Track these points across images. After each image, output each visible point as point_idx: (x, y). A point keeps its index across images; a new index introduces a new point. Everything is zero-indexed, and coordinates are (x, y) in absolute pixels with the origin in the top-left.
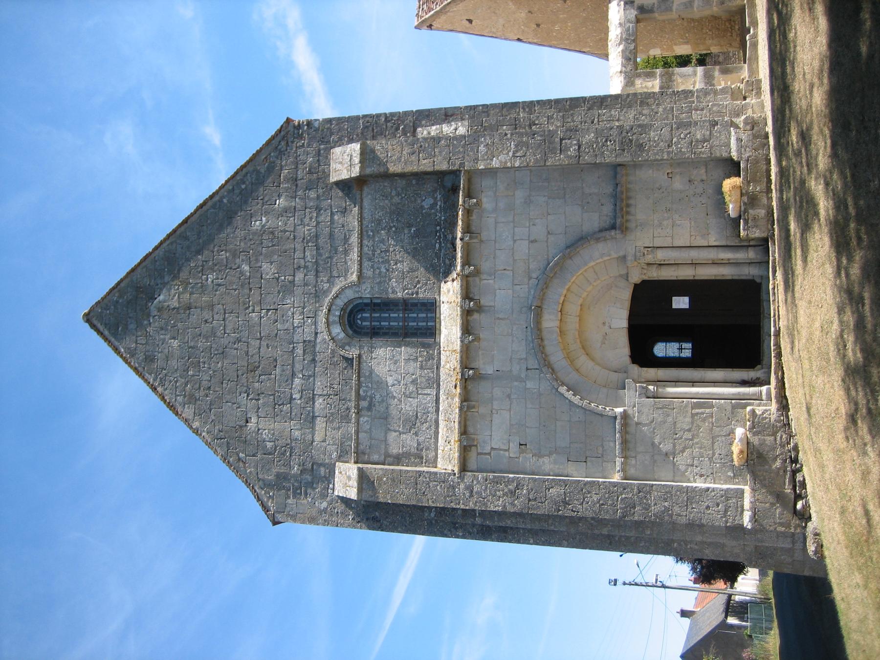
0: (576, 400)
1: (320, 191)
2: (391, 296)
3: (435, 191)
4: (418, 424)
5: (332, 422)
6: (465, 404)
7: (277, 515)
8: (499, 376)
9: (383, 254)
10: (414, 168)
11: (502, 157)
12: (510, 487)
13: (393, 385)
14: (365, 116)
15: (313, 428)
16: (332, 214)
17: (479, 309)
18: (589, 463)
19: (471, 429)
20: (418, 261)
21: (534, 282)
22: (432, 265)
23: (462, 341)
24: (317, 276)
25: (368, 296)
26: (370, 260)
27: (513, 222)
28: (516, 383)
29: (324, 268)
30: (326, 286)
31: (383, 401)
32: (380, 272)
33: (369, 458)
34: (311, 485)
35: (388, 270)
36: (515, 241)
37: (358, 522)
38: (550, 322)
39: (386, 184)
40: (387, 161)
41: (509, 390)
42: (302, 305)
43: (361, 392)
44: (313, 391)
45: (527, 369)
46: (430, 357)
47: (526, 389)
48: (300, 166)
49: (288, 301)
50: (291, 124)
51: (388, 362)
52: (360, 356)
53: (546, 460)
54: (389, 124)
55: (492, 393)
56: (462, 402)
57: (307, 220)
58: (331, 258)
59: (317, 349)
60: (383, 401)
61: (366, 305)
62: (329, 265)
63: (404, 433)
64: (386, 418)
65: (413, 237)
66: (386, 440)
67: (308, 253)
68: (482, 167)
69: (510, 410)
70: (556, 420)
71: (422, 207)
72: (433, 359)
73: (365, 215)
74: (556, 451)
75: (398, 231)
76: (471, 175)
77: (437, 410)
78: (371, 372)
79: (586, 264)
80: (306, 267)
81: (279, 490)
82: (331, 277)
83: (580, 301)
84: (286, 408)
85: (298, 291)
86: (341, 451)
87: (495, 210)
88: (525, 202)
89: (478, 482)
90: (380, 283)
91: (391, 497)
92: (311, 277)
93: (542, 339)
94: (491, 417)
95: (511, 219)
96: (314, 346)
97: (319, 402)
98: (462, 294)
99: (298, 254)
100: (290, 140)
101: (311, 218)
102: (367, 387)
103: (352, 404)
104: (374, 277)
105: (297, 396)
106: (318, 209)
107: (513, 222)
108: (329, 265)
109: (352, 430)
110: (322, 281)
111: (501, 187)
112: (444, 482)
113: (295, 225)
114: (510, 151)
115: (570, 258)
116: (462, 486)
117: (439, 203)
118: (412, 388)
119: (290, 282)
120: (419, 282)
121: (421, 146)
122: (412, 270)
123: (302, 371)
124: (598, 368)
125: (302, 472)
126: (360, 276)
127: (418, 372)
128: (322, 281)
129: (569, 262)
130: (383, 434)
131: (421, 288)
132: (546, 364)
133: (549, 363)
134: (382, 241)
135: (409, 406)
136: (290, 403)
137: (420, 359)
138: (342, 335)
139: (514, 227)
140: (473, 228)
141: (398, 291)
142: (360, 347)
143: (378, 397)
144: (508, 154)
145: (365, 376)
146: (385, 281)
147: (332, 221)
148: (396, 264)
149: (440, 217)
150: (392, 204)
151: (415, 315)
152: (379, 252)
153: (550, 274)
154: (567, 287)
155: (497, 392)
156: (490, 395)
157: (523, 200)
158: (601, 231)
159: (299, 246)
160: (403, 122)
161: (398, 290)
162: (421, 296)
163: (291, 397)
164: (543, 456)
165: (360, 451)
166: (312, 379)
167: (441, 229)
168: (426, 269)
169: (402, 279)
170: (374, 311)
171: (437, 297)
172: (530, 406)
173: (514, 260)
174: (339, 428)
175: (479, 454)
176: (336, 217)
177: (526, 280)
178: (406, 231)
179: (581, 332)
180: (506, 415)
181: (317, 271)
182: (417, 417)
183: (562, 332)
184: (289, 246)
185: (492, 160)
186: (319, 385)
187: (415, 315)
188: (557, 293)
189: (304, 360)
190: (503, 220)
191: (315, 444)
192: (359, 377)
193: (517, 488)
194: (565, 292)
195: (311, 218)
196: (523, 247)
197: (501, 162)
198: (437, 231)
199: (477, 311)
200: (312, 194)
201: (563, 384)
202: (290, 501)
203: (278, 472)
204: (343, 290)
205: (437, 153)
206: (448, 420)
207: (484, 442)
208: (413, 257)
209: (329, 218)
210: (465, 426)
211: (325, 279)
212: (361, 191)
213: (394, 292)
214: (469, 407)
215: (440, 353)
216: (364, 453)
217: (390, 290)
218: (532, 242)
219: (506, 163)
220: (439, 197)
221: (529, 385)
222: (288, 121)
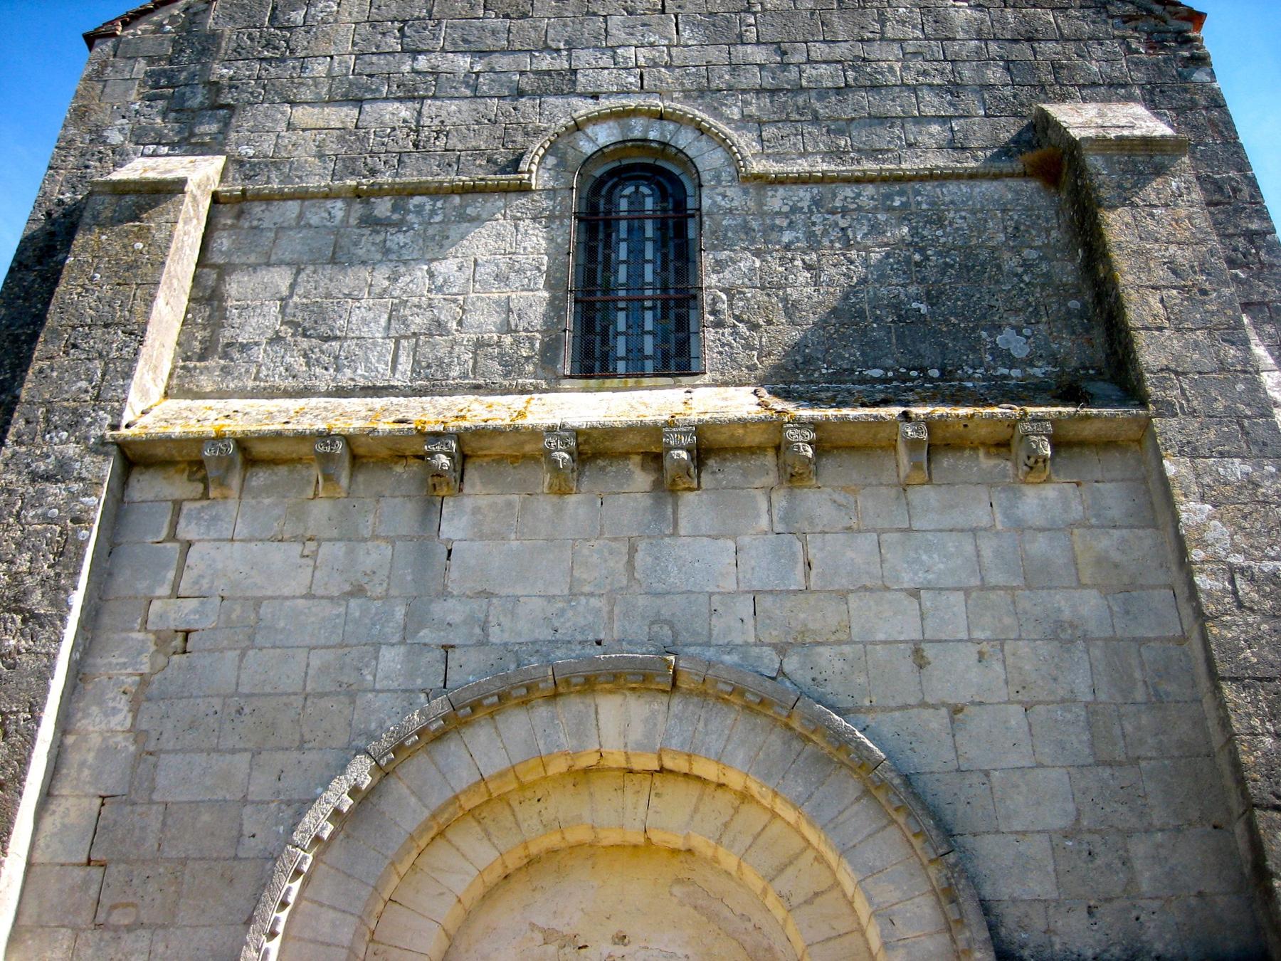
0: (318, 822)
1: (1008, 92)
2: (707, 259)
3: (1053, 359)
4: (305, 343)
5: (341, 139)
6: (340, 447)
7: (110, 42)
8: (429, 555)
9: (835, 234)
10: (1127, 273)
11: (1218, 531)
12: (37, 595)
13: (431, 275)
14: (1253, 183)
15: (331, 102)
16: (943, 120)
17: (668, 487)
18: (79, 874)
19: (260, 477)
20: (822, 324)
21: (769, 661)
22: (808, 360)
23: (551, 430)
24: (759, 91)
25: (706, 203)
26: (817, 203)
27: (984, 587)
28: (400, 612)
29: (783, 106)
30: (735, 113)
31: (387, 252)
32: (781, 229)
33: (225, 227)
34: (177, 109)
35: (787, 247)
36: (915, 593)
37: (49, 214)
38: (620, 724)
39: (1054, 234)
40: (1134, 205)
41: (379, 590)
42: (677, 62)
43: (417, 200)
44: (434, 97)
45: (446, 648)
46: (510, 366)
47: (377, 646)
48: (1071, 46)
49: (686, 34)
50: (1187, 25)
51: (508, 263)
52: (524, 189)
53: (122, 720)
54: (1241, 243)
55: (375, 537)
56: (348, 439)
57: (917, 64)
58: (816, 120)
59: (551, 100)
60: (387, 252)
61: (680, 205)
62: (795, 116)
63: (283, 309)
64: (333, 261)
65: (896, 306)
66: (268, 265)
67: (823, 69)
68: (1170, 468)
69: (309, 596)
70: (257, 753)
71: (998, 328)
72: (506, 375)
73: (952, 187)
74: (146, 752)
75: (912, 270)
76: (1143, 445)
77: (341, 392)
78: (477, 220)
79: (844, 852)
80: (784, 66)
81: (174, 42)
82: (761, 123)
83: (700, 842)
84: (393, 43)
85: (716, 54)
86: (253, 166)
87: (1020, 527)
88: (1060, 625)
89: (74, 496)
90: (747, 229)
91: (80, 265)
92: (754, 78)
93: (554, 696)
94: (295, 539)
95: (995, 578)
96: (559, 93)
97: (404, 111)
98: (715, 425)
99: (819, 50)
100: (1140, 24)
101: (925, 73)
102: (433, 212)
103: (385, 178)
104: (763, 214)
105: (422, 63)
106: (954, 88)
107: (984, 587)
108: (795, 116)
109: (313, 183)
110: (746, 103)
111: (1106, 543)
112: (97, 398)
113: (901, 41)
114: (1248, 556)
115: (866, 792)
116: (72, 449)
117: (1015, 373)
118: (419, 322)
119: (741, 36)
120: (754, 327)
121: (1204, 292)
122: (791, 309)
123: (492, 70)
124: (447, 912)
125: (215, 87)
126: (765, 181)
127: (468, 336)
128: (746, 103)
129: (852, 788)
130: (288, 257)
131: (735, 333)
132: (463, 714)
133: (466, 723)
134: (875, 229)
135: (364, 318)
136: (403, 51)
137: (508, 340)
138: (588, 148)
139: (967, 591)
140: (946, 461)
141: (721, 275)
142: (554, 190)
143: (401, 238)
144: (1236, 549)
145: (463, 206)
146: (753, 241)
147: (922, 120)
148: (808, 267)
149: (970, 378)
150: (994, 249)
151: (649, 326)
152: (843, 223)
153: (796, 716)
154: (755, 788)
155: (375, 556)
156: (367, 533)
157: (1067, 615)
158: (985, 907)
159: (841, 50)
160: (1259, 276)
161: (727, 274)
162: (710, 334)
163: (420, 52)
164: (135, 711)
165: (246, 206)
166: (468, 92)
167: (931, 380)
168: (798, 347)
169: (759, 286)
170: (662, 225)
171: (707, 378)
172: (315, 662)
173: (843, 595)
174: (321, 156)
175: (177, 505)
176: (935, 128)
177: (774, 635)
178: (912, 289)
179: (589, 851)
180: (296, 584)
181: (773, 92)
182: (327, 339)
183: (583, 776)
184: (840, 27)
185: (1203, 499)
186: (454, 110)
187: (649, 326)
188: (729, 751)
189: (522, 73)
190: (987, 553)
191: (287, 108)
192: (464, 190)
193: (30, 616)
194: (735, 780)
195: (925, 73)
196: (894, 622)
197: (1201, 528)
198: (922, 369)
199: (657, 485)
200: (995, 74)
201: (383, 773)
202: (141, 66)
203: (221, 36)
204: (723, 143)
205: (1190, 336)
206: (300, 413)
207: (215, 519)
208: (834, 311)
209: (930, 111)
210: (273, 462)
211: (753, 109)
212: (1024, 175)
213: (719, 266)
214: (326, 459)
215: (523, 391)
216: (239, 215)
217: (724, 255)
218: (917, 652)
219: (1202, 544)
220: (1038, 372)
221: (391, 659)
222: (1197, 18)
